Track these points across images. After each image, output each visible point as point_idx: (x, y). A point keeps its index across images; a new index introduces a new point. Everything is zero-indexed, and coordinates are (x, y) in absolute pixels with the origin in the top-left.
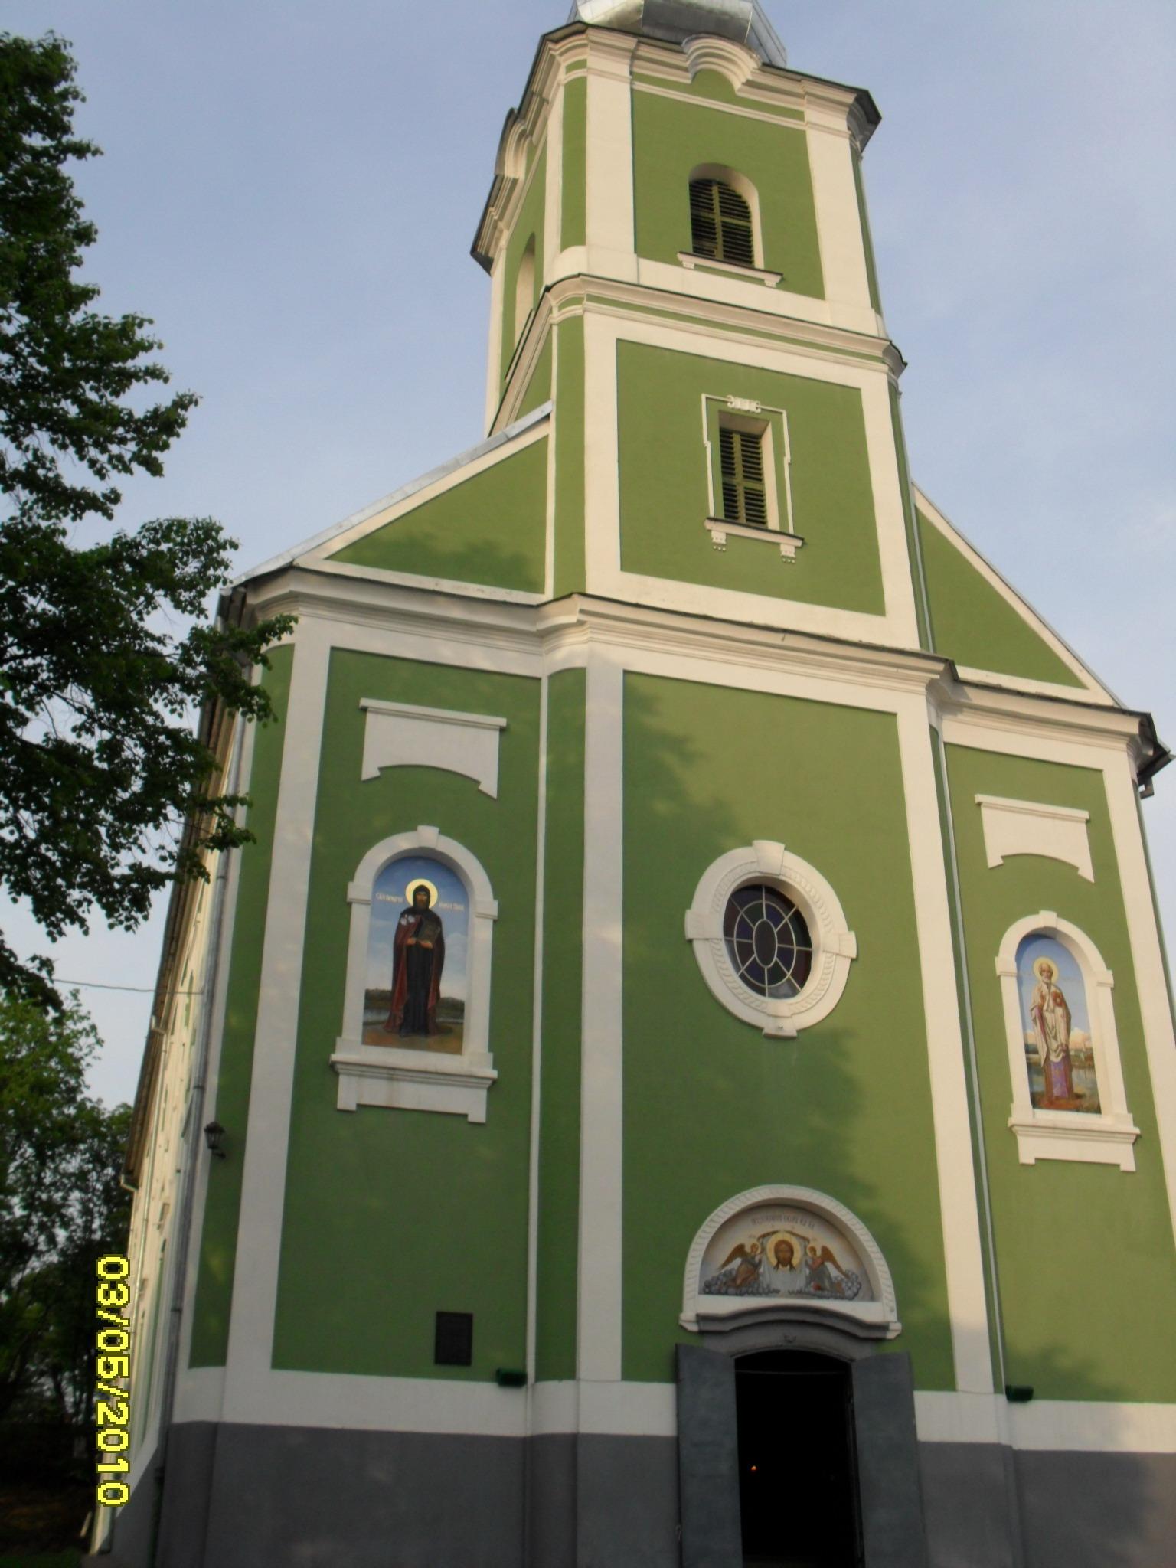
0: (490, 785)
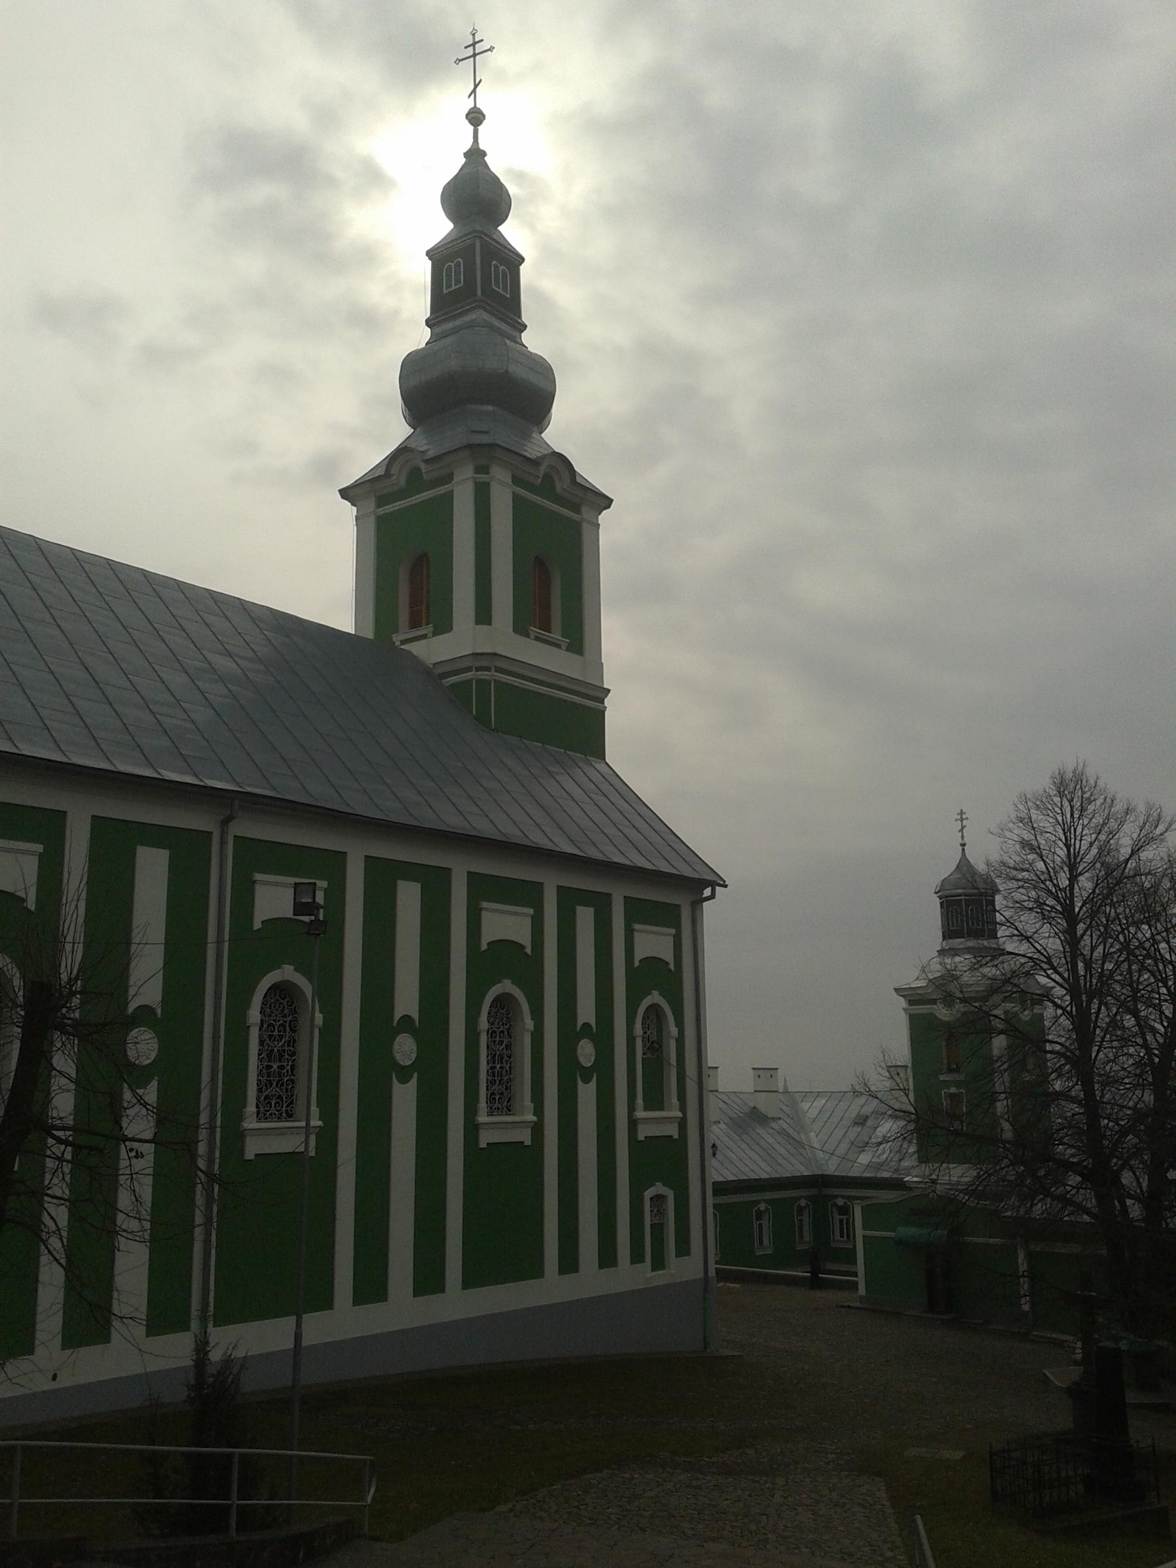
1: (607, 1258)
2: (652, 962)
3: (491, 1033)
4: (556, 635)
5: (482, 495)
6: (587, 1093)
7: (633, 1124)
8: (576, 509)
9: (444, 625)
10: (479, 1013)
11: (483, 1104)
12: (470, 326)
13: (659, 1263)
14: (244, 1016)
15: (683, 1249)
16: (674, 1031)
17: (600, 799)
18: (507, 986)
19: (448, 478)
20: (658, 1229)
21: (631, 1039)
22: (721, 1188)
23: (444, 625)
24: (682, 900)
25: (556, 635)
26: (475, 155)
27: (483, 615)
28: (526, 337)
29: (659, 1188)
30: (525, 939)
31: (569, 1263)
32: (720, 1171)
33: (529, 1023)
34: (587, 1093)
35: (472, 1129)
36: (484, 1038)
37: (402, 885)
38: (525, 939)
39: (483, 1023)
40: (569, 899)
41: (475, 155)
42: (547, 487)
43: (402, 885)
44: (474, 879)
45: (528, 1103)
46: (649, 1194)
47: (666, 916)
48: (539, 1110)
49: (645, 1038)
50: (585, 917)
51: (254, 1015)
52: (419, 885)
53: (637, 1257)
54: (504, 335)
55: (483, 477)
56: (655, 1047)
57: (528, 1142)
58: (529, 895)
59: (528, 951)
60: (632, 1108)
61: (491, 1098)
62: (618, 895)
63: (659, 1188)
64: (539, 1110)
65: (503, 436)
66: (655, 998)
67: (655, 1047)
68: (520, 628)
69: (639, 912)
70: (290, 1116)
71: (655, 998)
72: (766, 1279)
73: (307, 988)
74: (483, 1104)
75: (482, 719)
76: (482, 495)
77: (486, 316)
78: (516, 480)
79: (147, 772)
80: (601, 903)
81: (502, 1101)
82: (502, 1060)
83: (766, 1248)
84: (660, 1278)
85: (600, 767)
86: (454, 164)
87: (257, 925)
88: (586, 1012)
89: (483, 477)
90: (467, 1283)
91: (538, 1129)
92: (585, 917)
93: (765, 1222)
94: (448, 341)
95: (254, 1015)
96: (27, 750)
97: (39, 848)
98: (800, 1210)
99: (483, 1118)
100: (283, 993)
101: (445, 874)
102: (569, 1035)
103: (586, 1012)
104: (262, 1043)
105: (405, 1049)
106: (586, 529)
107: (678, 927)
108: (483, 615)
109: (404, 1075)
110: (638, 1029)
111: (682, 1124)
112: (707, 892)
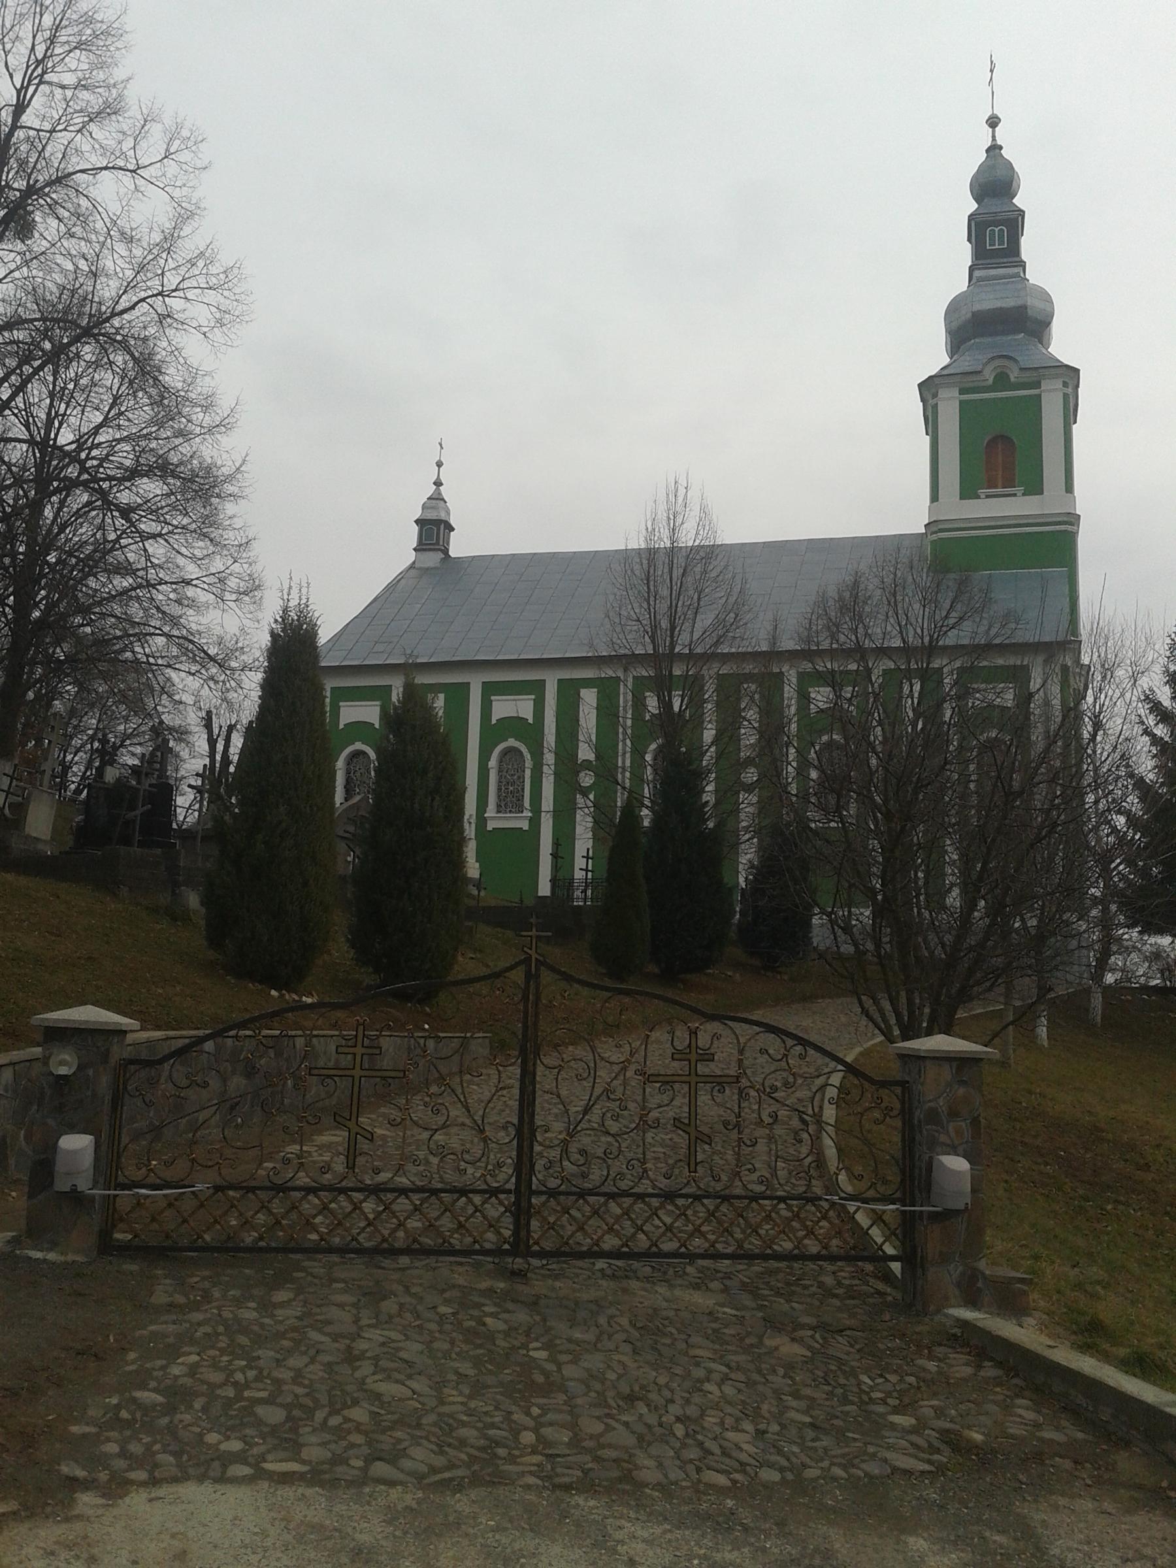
0: (531, 721)
26: (994, 149)
41: (994, 149)
73: (524, 750)
95: (493, 763)
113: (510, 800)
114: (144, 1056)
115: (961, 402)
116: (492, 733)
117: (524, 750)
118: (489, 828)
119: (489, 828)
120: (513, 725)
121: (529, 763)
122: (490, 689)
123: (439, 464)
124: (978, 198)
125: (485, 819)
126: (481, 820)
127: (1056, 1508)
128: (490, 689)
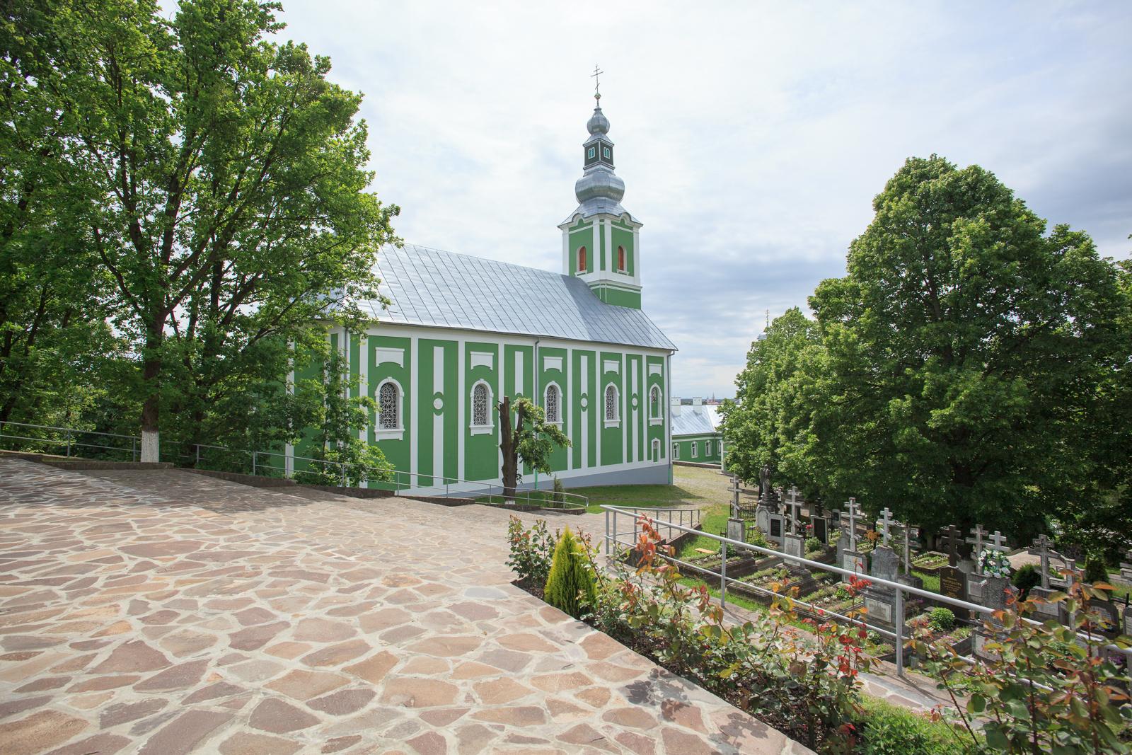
0: (402, 366)
1: (641, 458)
2: (553, 371)
3: (608, 397)
4: (625, 271)
5: (602, 228)
6: (635, 413)
7: (648, 422)
8: (631, 229)
9: (591, 271)
10: (470, 391)
11: (472, 421)
12: (598, 170)
13: (656, 460)
14: (469, 395)
15: (663, 456)
16: (661, 394)
17: (639, 324)
18: (612, 384)
19: (591, 223)
20: (656, 451)
21: (648, 398)
22: (675, 438)
23: (591, 271)
24: (664, 355)
25: (625, 271)
26: (598, 110)
27: (603, 268)
28: (615, 171)
29: (656, 439)
30: (401, 362)
31: (630, 459)
32: (674, 433)
33: (618, 394)
34: (635, 413)
35: (603, 424)
36: (605, 399)
37: (582, 357)
38: (401, 362)
39: (605, 395)
40: (629, 357)
41: (598, 110)
42: (622, 223)
43: (582, 357)
44: (602, 354)
45: (561, 418)
46: (653, 441)
47: (659, 360)
48: (621, 419)
49: (653, 397)
50: (634, 362)
51: (545, 395)
52: (443, 348)
53: (649, 458)
54: (610, 172)
55: (602, 223)
56: (655, 399)
57: (491, 434)
58: (617, 357)
59: (402, 366)
60: (648, 417)
61: (608, 415)
62: (644, 354)
63: (656, 439)
64: (621, 419)
65: (607, 210)
66: (655, 385)
67: (655, 399)
68: (614, 271)
69: (651, 360)
70: (395, 426)
71: (655, 385)
72: (693, 465)
73: (486, 383)
74: (472, 421)
75: (603, 301)
76: (602, 228)
77: (602, 167)
78: (612, 223)
79: (447, 326)
80: (639, 358)
81: (611, 416)
82: (610, 405)
83: (695, 456)
84: (656, 464)
85: (639, 312)
86: (590, 114)
87: (377, 365)
88: (635, 390)
89: (602, 223)
90: (574, 468)
91: (621, 424)
92: (634, 362)
93: (709, 446)
94: (591, 176)
95: (472, 394)
96: (452, 326)
97: (403, 350)
98: (707, 444)
99: (605, 421)
100: (481, 387)
101: (594, 353)
102: (577, 395)
103: (635, 390)
104: (475, 402)
105: (584, 402)
106: (635, 235)
107: (663, 364)
108: (603, 268)
109: (438, 412)
110: (650, 395)
111: (663, 421)
112: (672, 352)
113: (390, 421)
114: (745, 597)
115: (570, 235)
116: (377, 372)
117: (486, 383)
118: (472, 435)
119: (472, 435)
120: (390, 368)
121: (401, 393)
122: (470, 347)
123: (598, 97)
124: (591, 132)
125: (470, 429)
126: (603, 424)
127: (411, 519)
128: (470, 347)
